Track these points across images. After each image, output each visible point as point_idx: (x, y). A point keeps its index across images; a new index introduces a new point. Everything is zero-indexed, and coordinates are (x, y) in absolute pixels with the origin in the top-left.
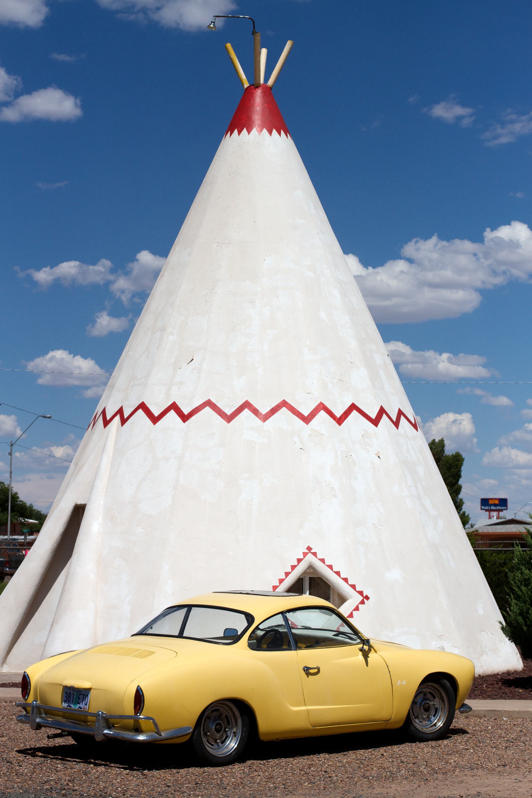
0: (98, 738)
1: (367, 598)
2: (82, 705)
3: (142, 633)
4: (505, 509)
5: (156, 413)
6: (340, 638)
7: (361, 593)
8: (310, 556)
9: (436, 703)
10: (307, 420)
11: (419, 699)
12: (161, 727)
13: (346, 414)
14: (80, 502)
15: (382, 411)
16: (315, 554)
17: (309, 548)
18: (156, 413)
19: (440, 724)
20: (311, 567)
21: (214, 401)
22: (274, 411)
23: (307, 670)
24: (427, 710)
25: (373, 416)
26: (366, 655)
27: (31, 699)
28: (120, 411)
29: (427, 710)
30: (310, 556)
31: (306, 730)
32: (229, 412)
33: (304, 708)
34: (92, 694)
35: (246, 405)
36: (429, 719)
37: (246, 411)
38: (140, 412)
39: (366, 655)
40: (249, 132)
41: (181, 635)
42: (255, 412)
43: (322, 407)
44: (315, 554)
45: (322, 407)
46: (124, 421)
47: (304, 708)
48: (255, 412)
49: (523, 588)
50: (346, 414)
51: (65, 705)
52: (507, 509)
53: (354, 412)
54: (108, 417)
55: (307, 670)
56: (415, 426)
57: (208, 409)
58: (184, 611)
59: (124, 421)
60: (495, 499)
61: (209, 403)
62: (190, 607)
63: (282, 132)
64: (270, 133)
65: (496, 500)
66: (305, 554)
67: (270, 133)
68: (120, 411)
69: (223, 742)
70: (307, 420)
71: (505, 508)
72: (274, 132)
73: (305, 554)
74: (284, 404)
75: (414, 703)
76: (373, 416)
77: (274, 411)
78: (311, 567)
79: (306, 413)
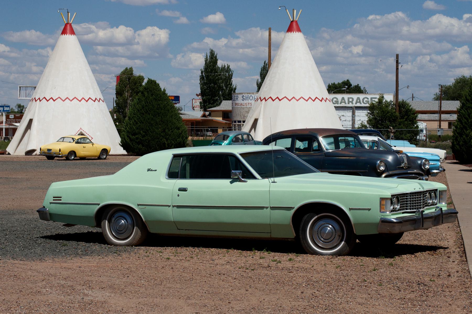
0: (54, 156)
1: (93, 138)
2: (51, 152)
3: (57, 141)
4: (178, 103)
5: (48, 99)
6: (89, 143)
7: (91, 137)
8: (81, 130)
9: (104, 153)
10: (80, 101)
11: (101, 153)
12: (63, 154)
13: (88, 100)
14: (31, 118)
15: (96, 99)
16: (82, 129)
17: (81, 128)
18: (277, 99)
19: (105, 157)
20: (81, 132)
21: (60, 97)
22: (73, 99)
23: (84, 147)
24: (103, 155)
25: (94, 100)
26: (93, 145)
27: (41, 151)
28: (39, 99)
29: (103, 155)
30: (81, 130)
31: (83, 156)
32: (64, 99)
33: (83, 153)
34: (52, 150)
35: (67, 98)
36: (103, 156)
37: (67, 99)
38: (44, 99)
39: (93, 145)
40: (67, 35)
41: (63, 141)
42: (69, 99)
43: (83, 98)
44: (82, 129)
45: (83, 98)
46: (40, 101)
47: (83, 153)
48: (69, 99)
49: (123, 136)
50: (88, 100)
51: (48, 152)
52: (179, 103)
53: (307, 99)
54: (36, 100)
55: (84, 147)
56: (103, 101)
57: (59, 99)
58: (63, 138)
59: (40, 101)
60: (172, 96)
61: (59, 98)
62: (64, 138)
63: (74, 35)
64: (71, 35)
65: (172, 97)
66: (80, 129)
67: (71, 35)
68: (39, 99)
69: (71, 157)
70: (80, 101)
71: (178, 102)
72: (72, 35)
73: (80, 129)
74: (75, 98)
75: (100, 153)
76: (94, 100)
77: (73, 99)
78: (81, 132)
79: (80, 100)
